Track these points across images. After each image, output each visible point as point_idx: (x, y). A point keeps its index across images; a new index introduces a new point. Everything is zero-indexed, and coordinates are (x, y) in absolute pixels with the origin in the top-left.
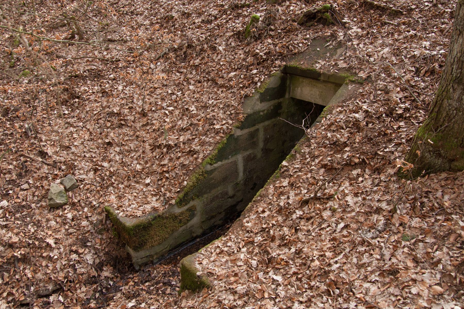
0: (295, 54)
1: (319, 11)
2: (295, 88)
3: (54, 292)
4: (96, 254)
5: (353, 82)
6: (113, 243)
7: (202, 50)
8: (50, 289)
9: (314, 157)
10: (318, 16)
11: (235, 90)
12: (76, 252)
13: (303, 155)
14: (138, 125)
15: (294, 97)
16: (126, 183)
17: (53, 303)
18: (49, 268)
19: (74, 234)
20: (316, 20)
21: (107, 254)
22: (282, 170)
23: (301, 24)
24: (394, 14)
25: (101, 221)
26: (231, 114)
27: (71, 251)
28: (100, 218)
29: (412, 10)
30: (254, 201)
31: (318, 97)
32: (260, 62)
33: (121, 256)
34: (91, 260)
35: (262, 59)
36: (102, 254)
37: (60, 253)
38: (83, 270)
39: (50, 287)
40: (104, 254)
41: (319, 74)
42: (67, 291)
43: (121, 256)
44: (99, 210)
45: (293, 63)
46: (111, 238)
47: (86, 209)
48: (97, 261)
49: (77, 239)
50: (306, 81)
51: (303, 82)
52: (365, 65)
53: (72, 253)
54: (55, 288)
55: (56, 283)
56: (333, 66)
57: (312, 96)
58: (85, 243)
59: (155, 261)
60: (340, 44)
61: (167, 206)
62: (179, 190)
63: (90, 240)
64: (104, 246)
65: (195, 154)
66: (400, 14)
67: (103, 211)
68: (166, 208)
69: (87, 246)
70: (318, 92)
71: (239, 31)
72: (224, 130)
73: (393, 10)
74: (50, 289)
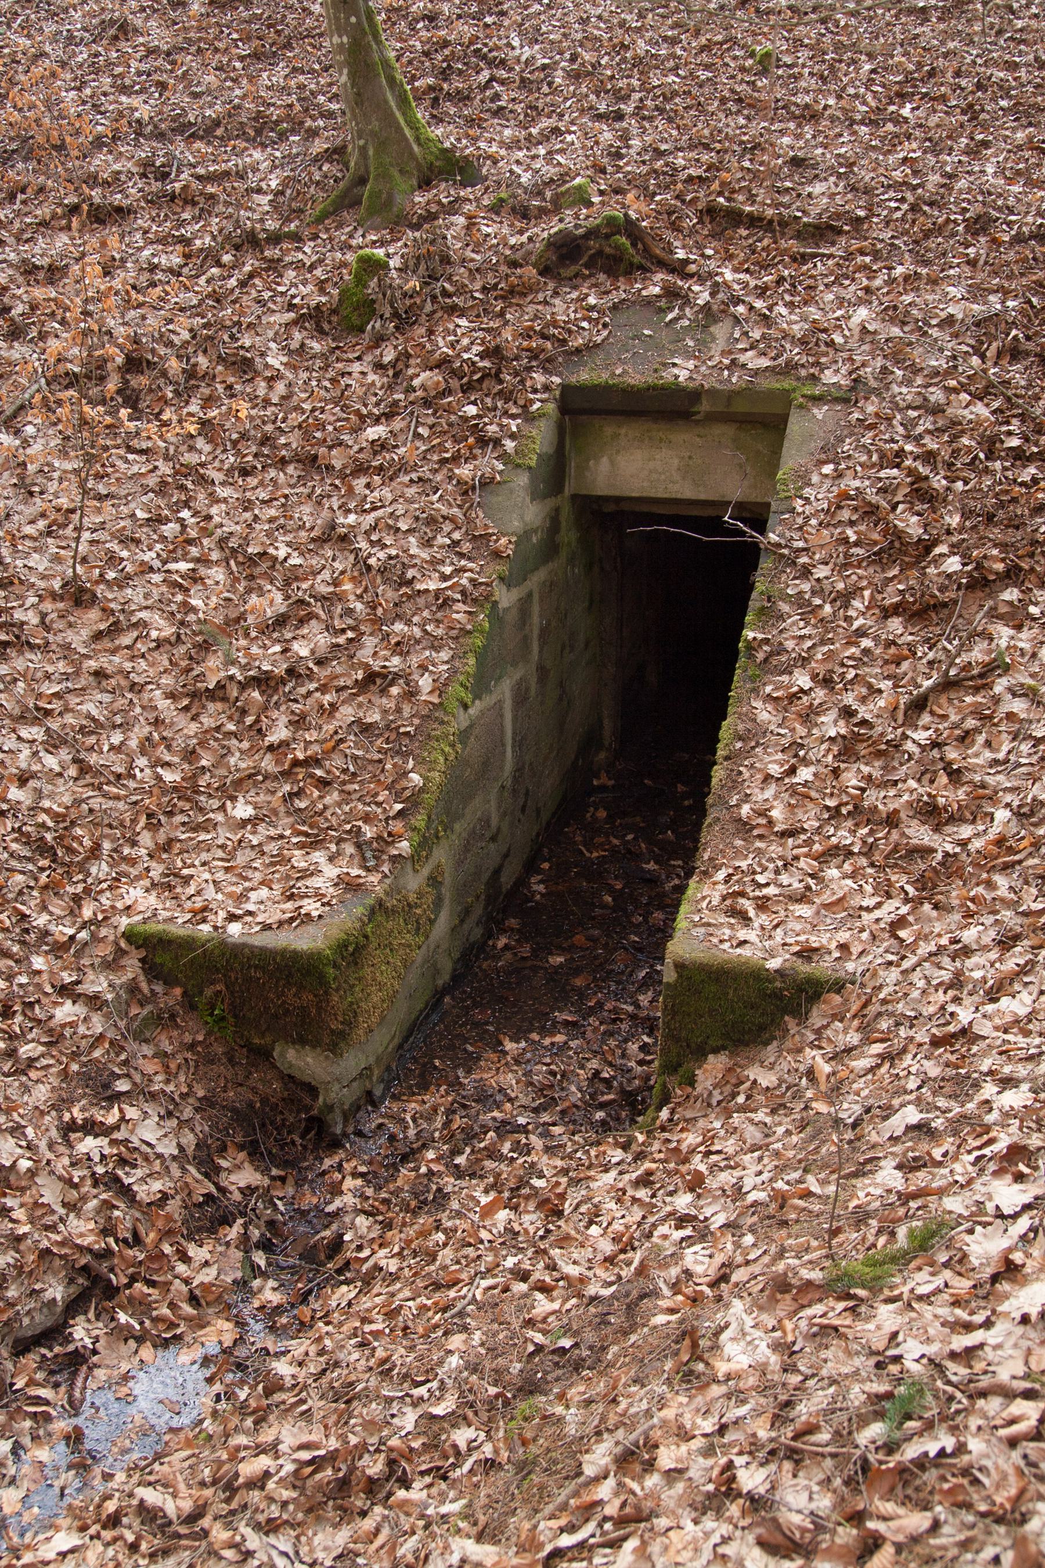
0: (578, 351)
1: (592, 233)
2: (588, 460)
3: (74, 1306)
4: (170, 1114)
5: (818, 400)
6: (212, 1062)
7: (191, 373)
8: (59, 1297)
9: (844, 599)
10: (589, 248)
11: (425, 471)
12: (91, 1128)
13: (799, 602)
14: (78, 639)
15: (584, 492)
16: (146, 839)
17: (95, 1352)
18: (15, 1215)
19: (44, 1062)
20: (585, 259)
21: (206, 1104)
22: (760, 656)
23: (545, 271)
24: (813, 235)
25: (133, 988)
26: (456, 543)
27: (69, 1129)
28: (122, 979)
29: (859, 219)
30: (727, 758)
31: (677, 477)
32: (469, 382)
33: (264, 1101)
34: (166, 1141)
35: (474, 373)
36: (188, 1113)
37: (29, 1147)
38: (157, 1186)
39: (56, 1291)
40: (197, 1110)
41: (695, 395)
42: (129, 1285)
43: (264, 1101)
44: (105, 951)
45: (584, 376)
46: (192, 1047)
47: (38, 962)
48: (189, 1139)
49: (65, 1074)
50: (628, 431)
51: (616, 436)
52: (826, 354)
53: (73, 1136)
54: (73, 1290)
55: (74, 1272)
56: (728, 368)
57: (655, 476)
58: (106, 1086)
59: (378, 1092)
60: (709, 315)
61: (385, 869)
62: (398, 807)
63: (117, 1070)
64: (182, 1078)
65: (392, 684)
66: (830, 235)
67: (120, 952)
68: (386, 876)
69: (118, 1096)
70: (676, 461)
71: (318, 307)
72: (463, 593)
73: (805, 225)
74: (59, 1297)
